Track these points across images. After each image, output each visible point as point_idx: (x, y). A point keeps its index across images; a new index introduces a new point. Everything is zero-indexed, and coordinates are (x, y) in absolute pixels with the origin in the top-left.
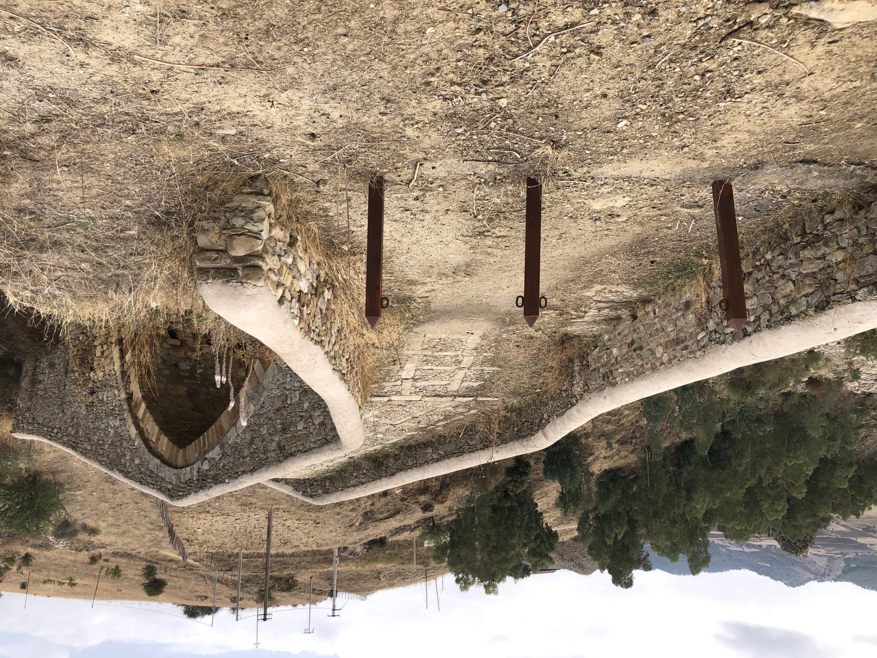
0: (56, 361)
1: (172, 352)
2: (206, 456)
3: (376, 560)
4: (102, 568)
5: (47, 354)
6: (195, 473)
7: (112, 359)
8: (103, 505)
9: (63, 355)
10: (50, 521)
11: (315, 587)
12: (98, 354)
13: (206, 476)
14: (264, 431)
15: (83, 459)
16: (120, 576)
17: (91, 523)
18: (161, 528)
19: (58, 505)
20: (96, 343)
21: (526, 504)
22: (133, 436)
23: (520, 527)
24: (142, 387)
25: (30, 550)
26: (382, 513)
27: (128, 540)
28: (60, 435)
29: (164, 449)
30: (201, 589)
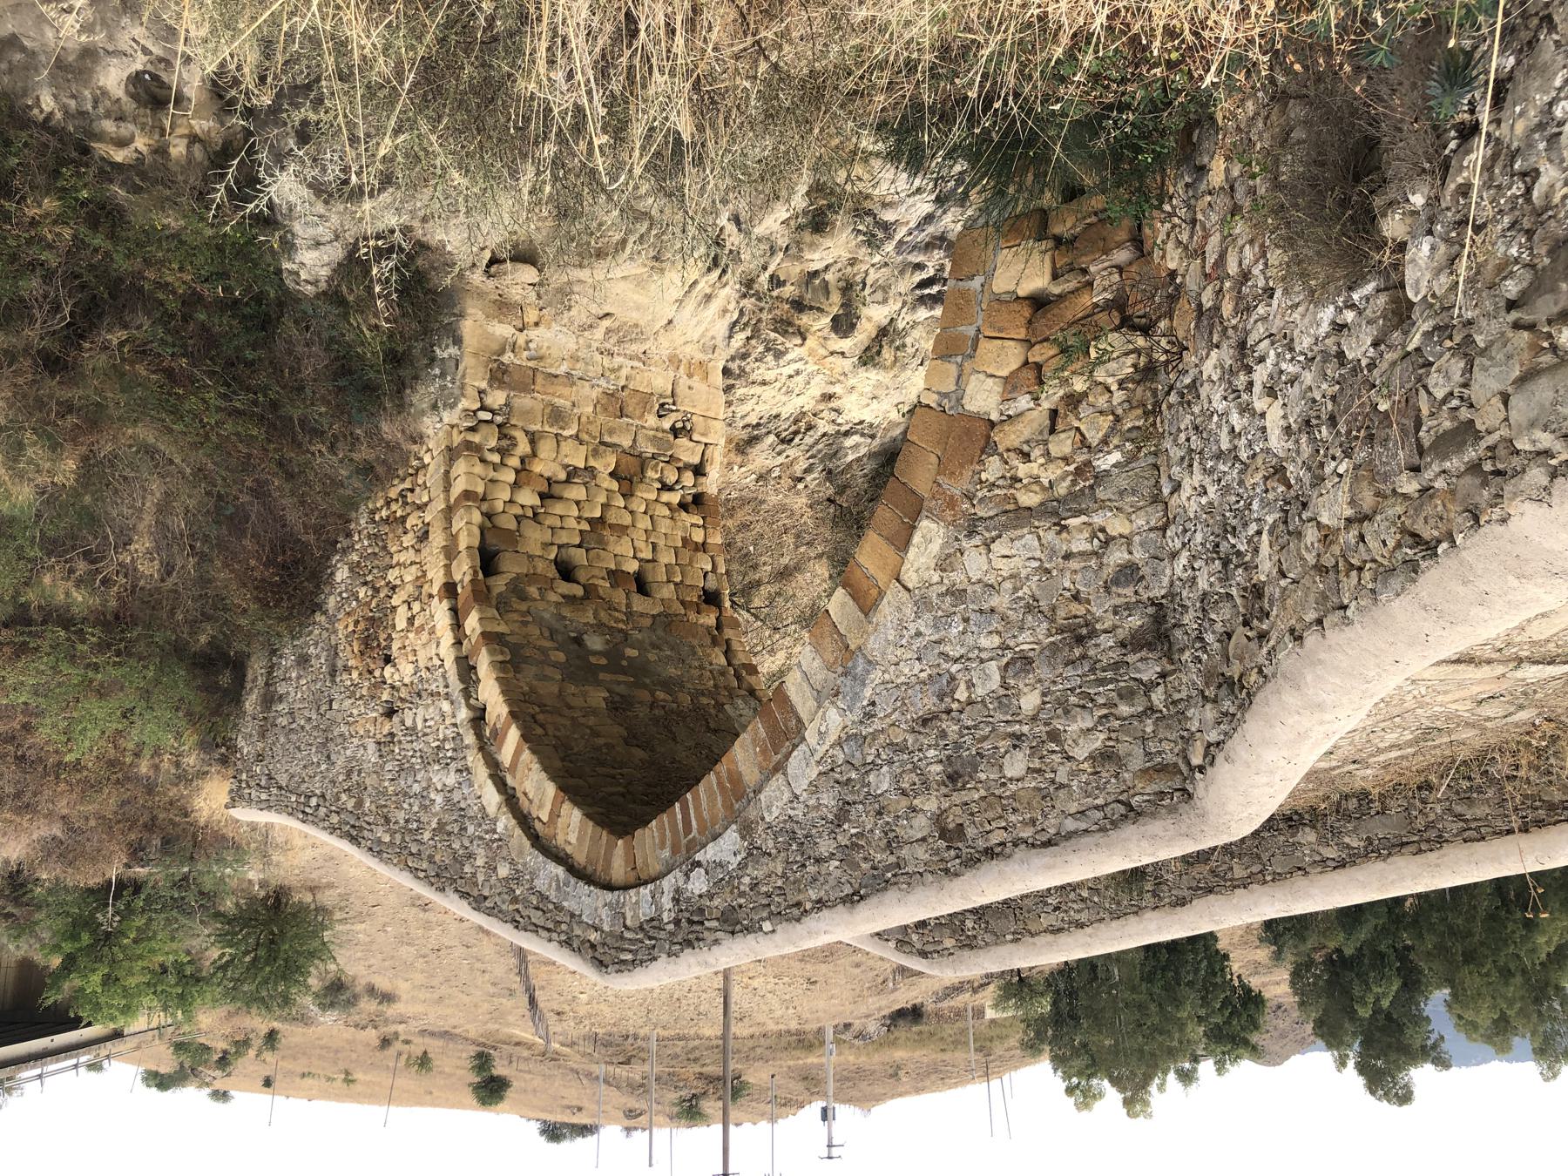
0: (312, 650)
1: (566, 612)
2: (698, 857)
3: (894, 1044)
4: (400, 1054)
5: (293, 638)
7: (432, 632)
8: (406, 952)
9: (325, 634)
10: (308, 987)
11: (778, 1093)
12: (401, 623)
13: (701, 911)
14: (882, 782)
15: (373, 863)
16: (430, 1069)
17: (382, 983)
18: (512, 993)
19: (321, 952)
20: (395, 601)
22: (491, 810)
23: (1190, 984)
24: (507, 690)
25: (276, 1025)
27: (449, 1011)
28: (322, 811)
29: (573, 838)
30: (573, 1094)
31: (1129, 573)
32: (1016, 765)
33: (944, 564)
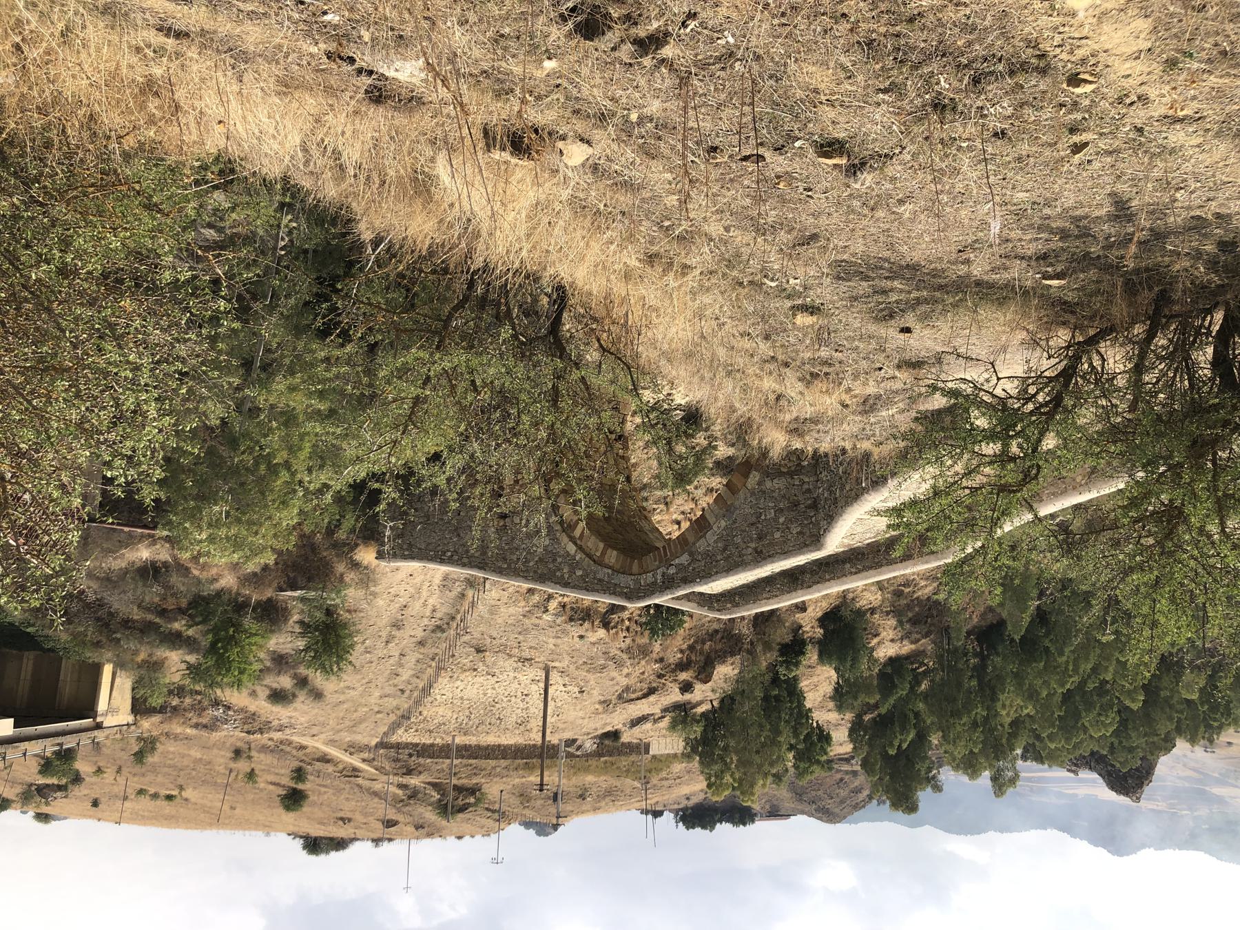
6: (659, 577)
14: (738, 540)
21: (793, 692)
22: (572, 552)
26: (634, 691)
31: (809, 491)
32: (777, 535)
33: (759, 483)
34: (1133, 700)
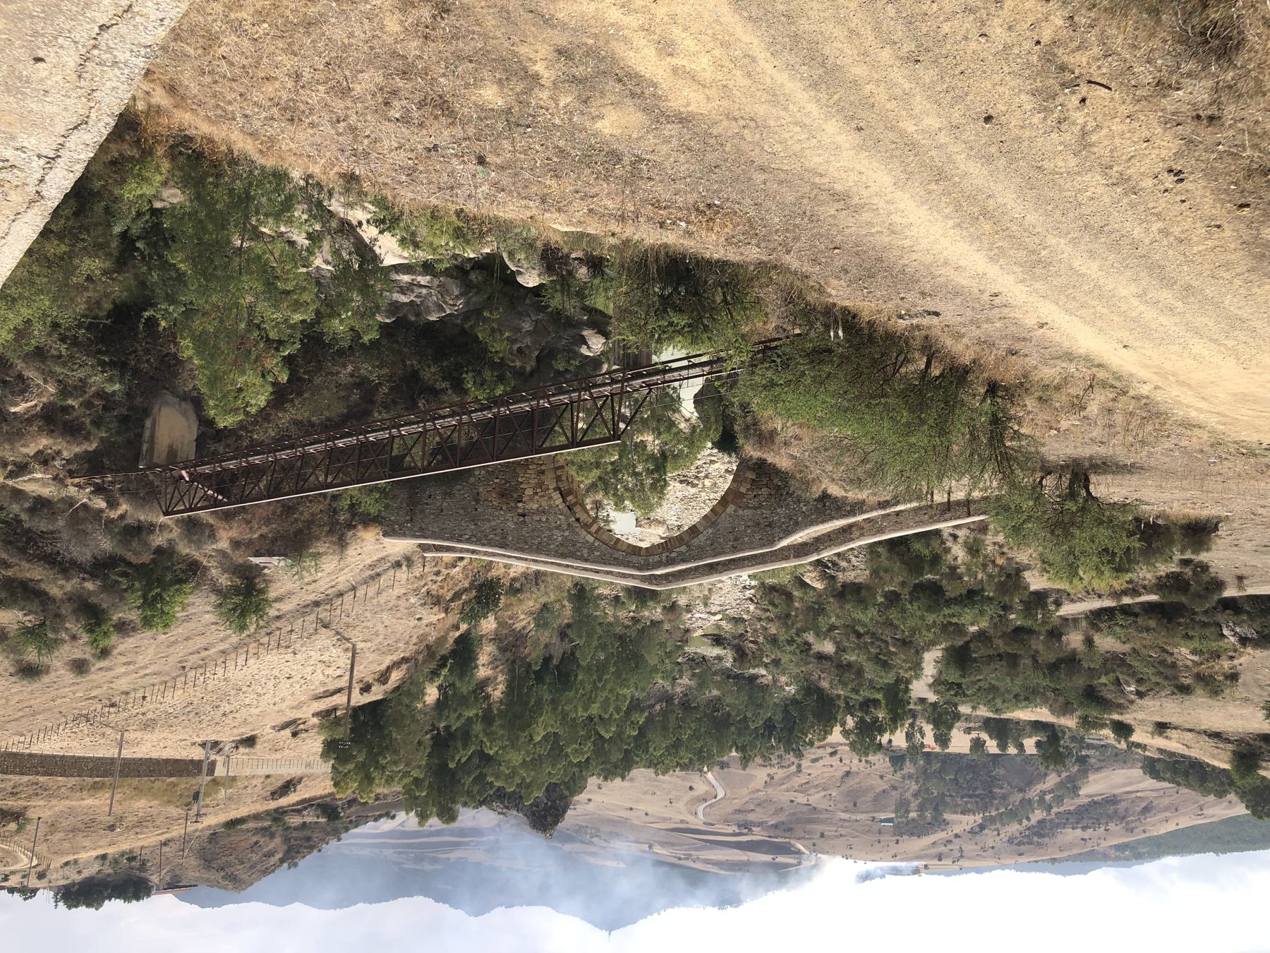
34: (607, 732)
